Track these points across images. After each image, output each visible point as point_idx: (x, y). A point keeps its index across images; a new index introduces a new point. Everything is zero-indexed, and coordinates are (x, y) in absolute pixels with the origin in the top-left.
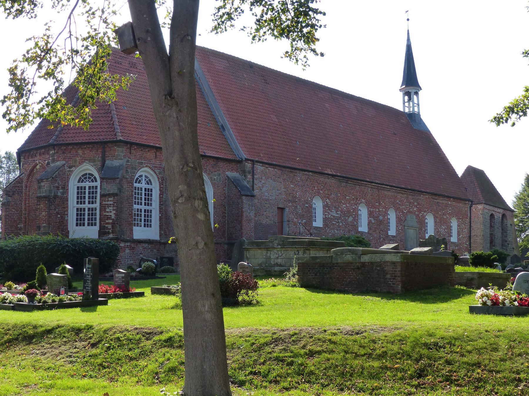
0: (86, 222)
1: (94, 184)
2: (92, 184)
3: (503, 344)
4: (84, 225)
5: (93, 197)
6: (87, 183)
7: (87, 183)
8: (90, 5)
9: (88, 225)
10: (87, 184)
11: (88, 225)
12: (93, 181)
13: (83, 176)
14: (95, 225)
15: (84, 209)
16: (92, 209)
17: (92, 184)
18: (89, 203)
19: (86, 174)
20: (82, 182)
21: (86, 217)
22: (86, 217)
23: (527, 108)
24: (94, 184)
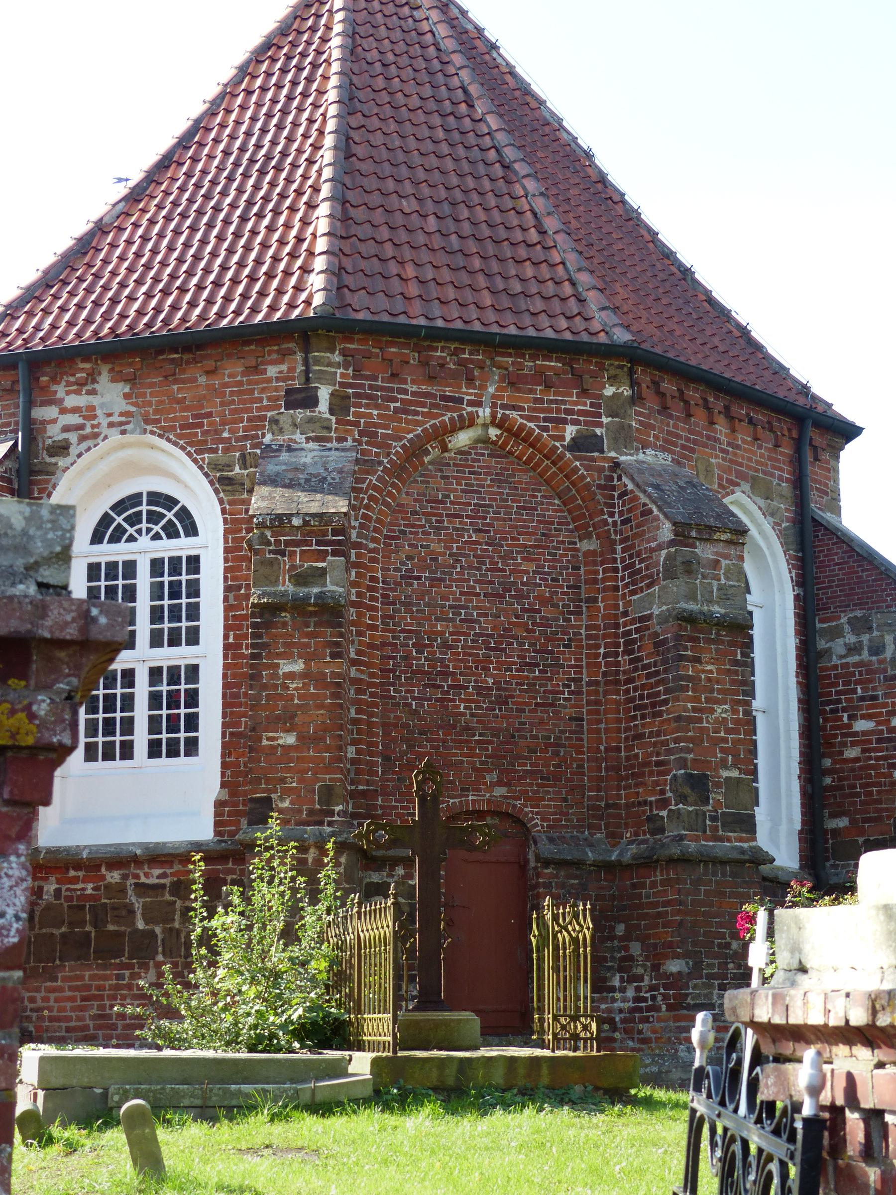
0: (141, 737)
1: (182, 547)
2: (168, 548)
3: (883, 568)
4: (127, 752)
5: (175, 594)
6: (144, 541)
7: (144, 541)
8: (96, 386)
9: (154, 750)
10: (144, 550)
11: (154, 750)
12: (171, 532)
13: (120, 506)
14: (192, 747)
15: (130, 568)
16: (175, 563)
17: (168, 548)
18: (156, 640)
19: (135, 499)
20: (115, 538)
21: (141, 713)
22: (141, 713)
23: (892, 766)
24: (182, 547)
